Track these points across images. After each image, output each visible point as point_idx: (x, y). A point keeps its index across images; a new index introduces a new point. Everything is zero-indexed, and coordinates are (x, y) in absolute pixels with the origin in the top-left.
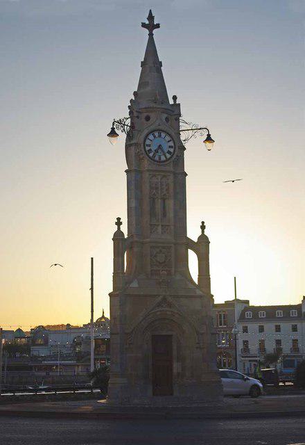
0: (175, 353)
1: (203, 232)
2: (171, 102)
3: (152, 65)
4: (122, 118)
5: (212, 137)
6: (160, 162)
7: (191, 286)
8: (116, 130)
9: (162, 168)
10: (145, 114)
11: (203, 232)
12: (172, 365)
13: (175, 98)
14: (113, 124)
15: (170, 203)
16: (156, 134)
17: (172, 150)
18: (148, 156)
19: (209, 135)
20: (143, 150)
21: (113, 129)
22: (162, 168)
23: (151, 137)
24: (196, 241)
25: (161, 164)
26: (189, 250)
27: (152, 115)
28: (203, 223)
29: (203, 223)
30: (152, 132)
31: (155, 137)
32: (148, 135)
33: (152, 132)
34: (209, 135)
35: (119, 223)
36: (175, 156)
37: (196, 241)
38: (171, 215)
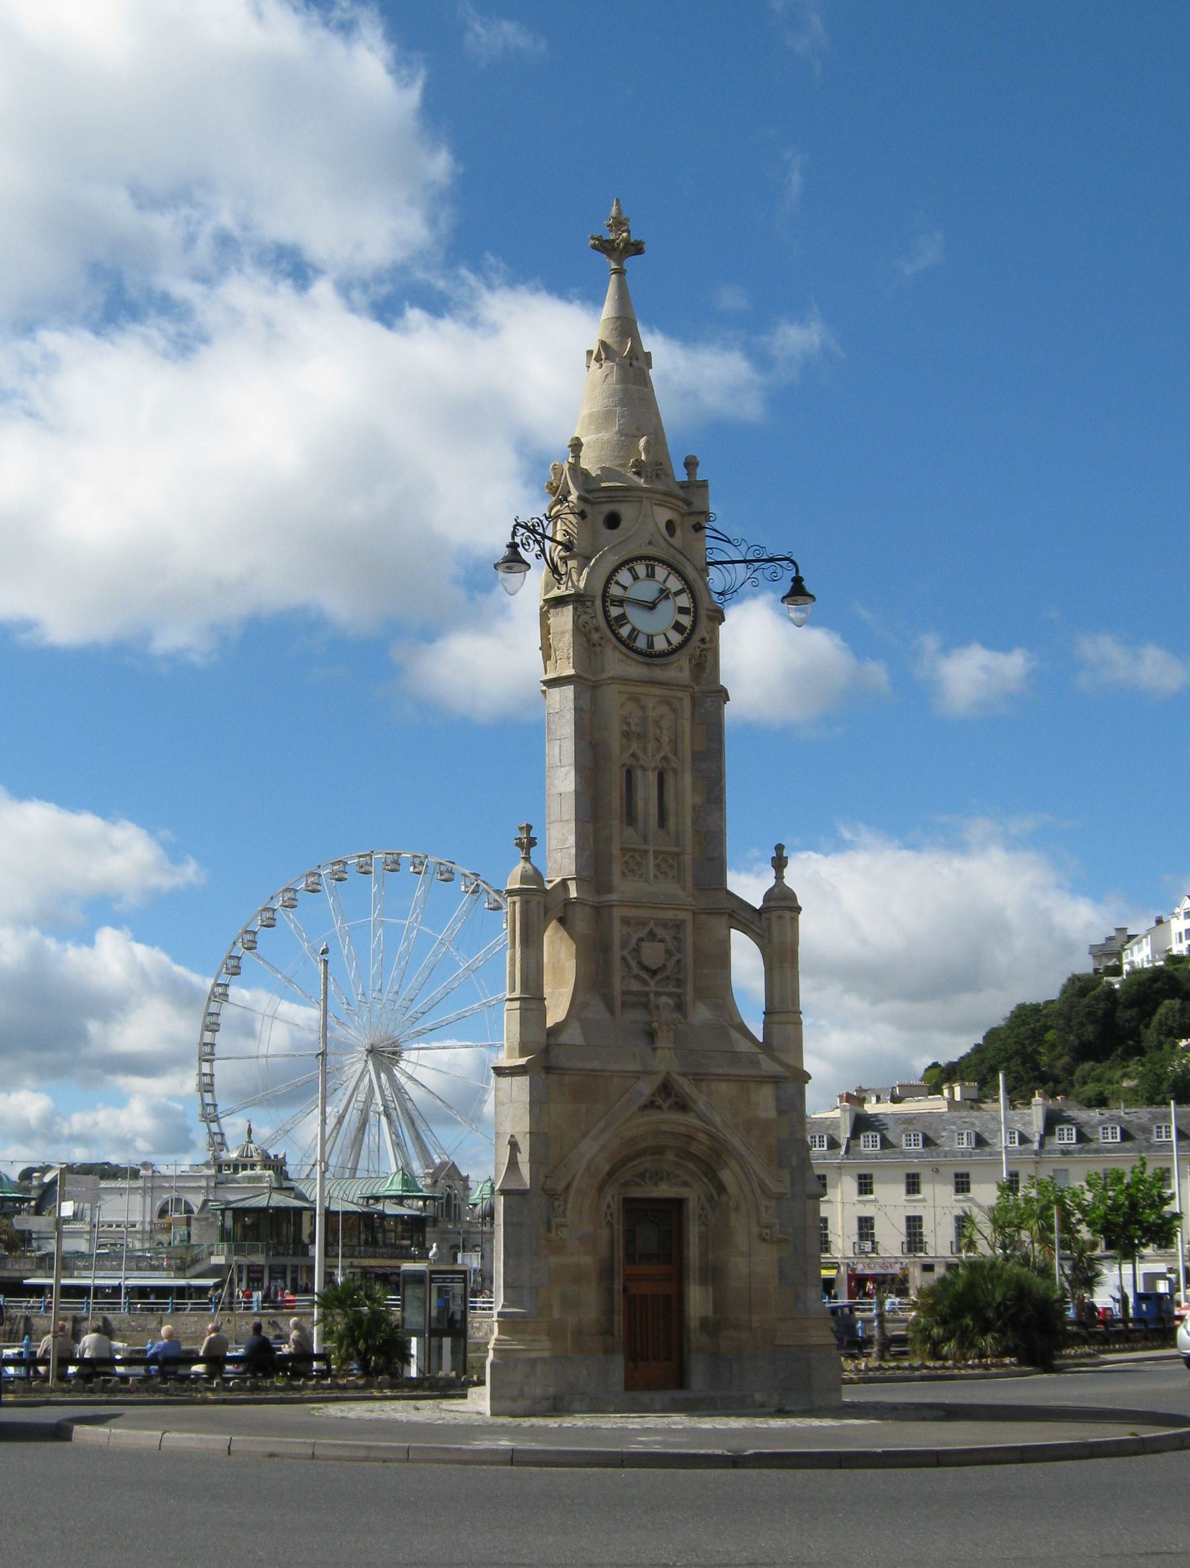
0: (693, 1252)
1: (779, 877)
2: (681, 475)
3: (250, 1125)
4: (631, 226)
5: (808, 585)
6: (650, 656)
7: (744, 1046)
8: (520, 549)
9: (659, 674)
10: (607, 508)
11: (779, 877)
12: (681, 1297)
13: (691, 464)
14: (514, 534)
15: (685, 786)
16: (641, 569)
17: (686, 621)
18: (616, 635)
19: (797, 581)
20: (600, 616)
21: (513, 546)
22: (659, 674)
23: (624, 577)
24: (757, 903)
25: (657, 661)
26: (734, 933)
27: (627, 512)
28: (779, 848)
29: (779, 848)
30: (628, 563)
31: (636, 578)
32: (616, 570)
33: (628, 563)
34: (797, 581)
35: (514, 1146)
36: (696, 638)
37: (757, 903)
38: (684, 819)
